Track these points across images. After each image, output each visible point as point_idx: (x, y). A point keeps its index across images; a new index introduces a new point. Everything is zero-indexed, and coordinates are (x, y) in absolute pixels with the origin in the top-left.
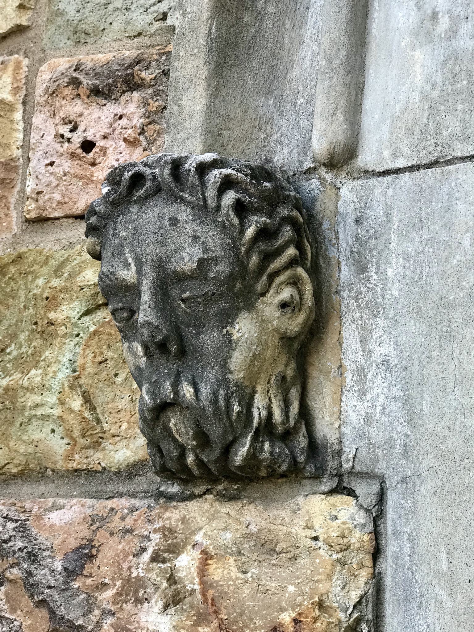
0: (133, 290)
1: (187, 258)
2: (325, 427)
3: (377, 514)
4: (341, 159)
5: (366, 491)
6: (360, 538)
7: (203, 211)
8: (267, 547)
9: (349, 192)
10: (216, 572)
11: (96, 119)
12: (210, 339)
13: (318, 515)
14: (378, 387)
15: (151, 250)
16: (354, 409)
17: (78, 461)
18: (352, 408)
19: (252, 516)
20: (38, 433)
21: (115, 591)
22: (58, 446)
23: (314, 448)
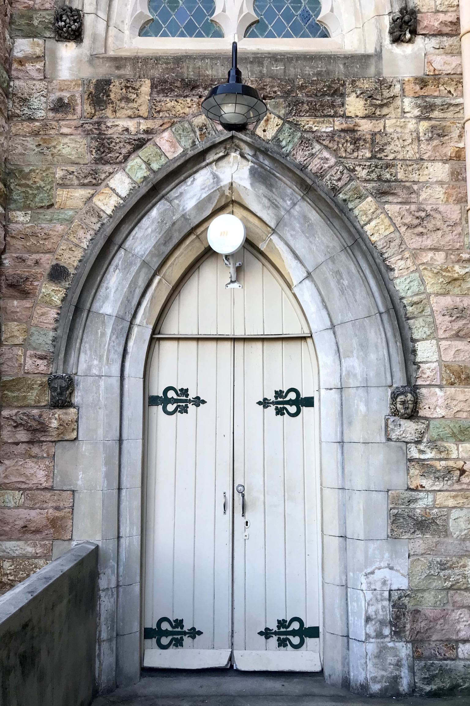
0: (57, 388)
1: (64, 385)
2: (73, 402)
3: (78, 410)
4: (76, 374)
5: (77, 408)
6: (77, 412)
7: (65, 381)
8: (66, 414)
9: (76, 377)
10: (60, 416)
11: (39, 362)
12: (64, 393)
13: (72, 410)
14: (79, 398)
15: (59, 384)
16: (76, 400)
17: (36, 405)
18: (77, 399)
19: (64, 411)
20: (29, 401)
21: (356, 350)
22: (33, 403)
23: (72, 404)
